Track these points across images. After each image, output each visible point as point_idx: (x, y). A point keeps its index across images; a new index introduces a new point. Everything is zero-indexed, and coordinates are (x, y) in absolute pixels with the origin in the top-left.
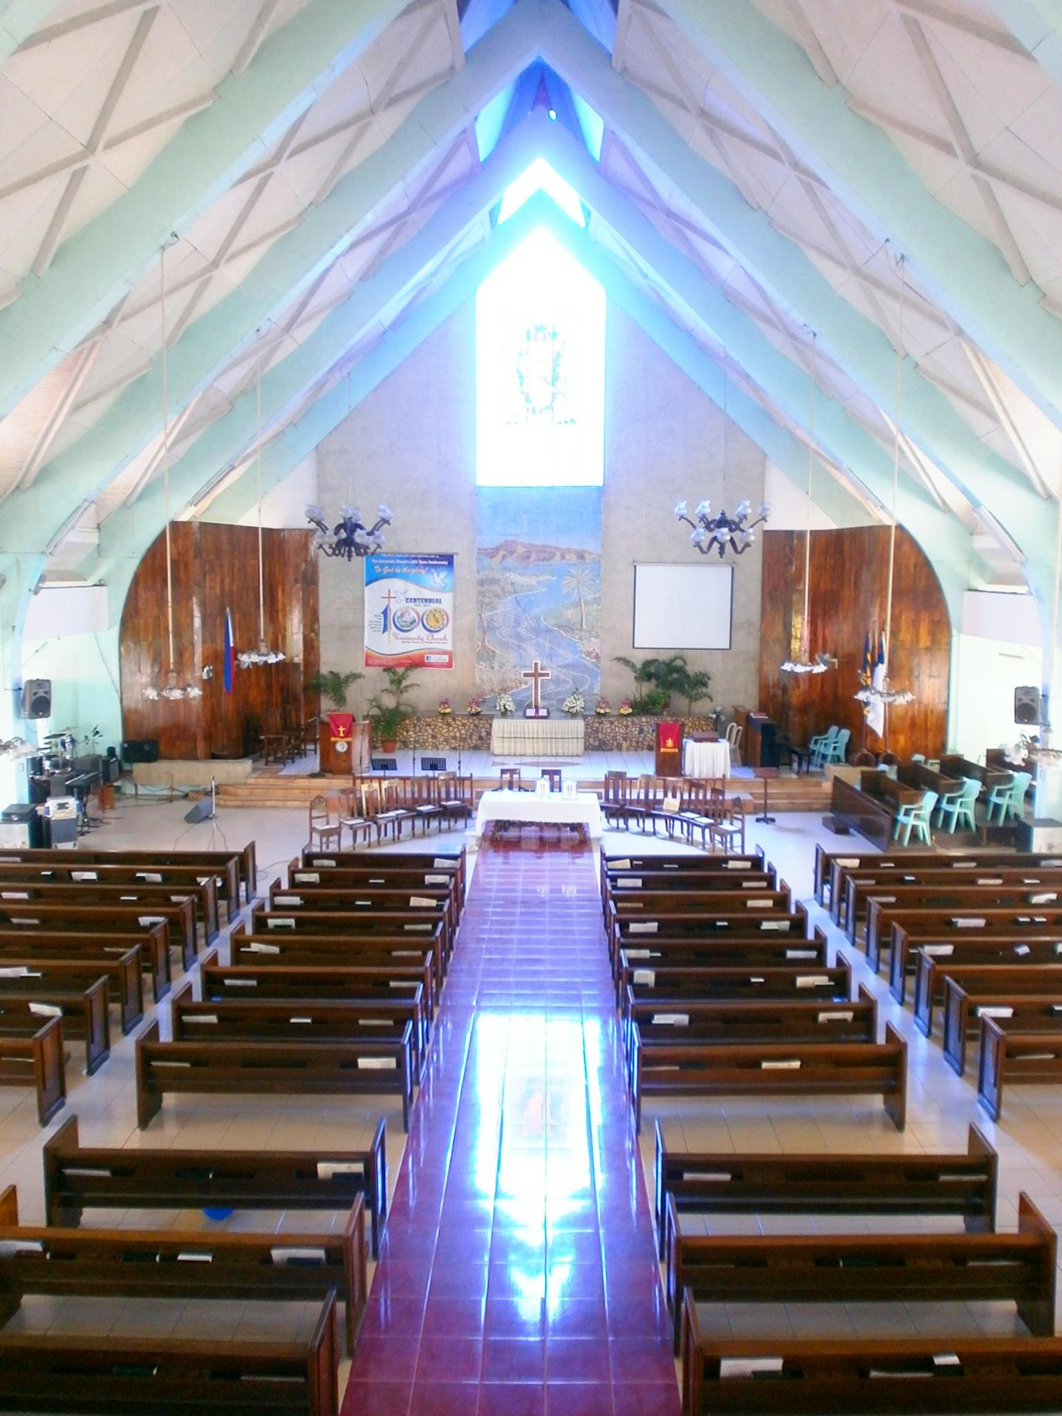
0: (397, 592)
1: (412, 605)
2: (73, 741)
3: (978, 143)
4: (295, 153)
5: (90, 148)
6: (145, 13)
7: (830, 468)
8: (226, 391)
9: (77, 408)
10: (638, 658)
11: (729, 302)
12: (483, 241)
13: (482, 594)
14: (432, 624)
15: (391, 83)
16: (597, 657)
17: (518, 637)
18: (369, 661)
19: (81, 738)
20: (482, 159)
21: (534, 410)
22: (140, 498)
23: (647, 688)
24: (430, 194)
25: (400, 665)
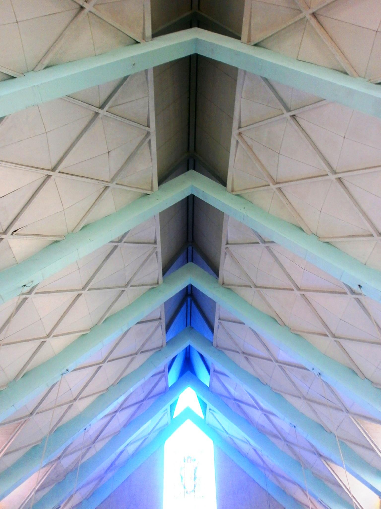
3: (333, 330)
4: (108, 362)
5: (48, 336)
6: (79, 294)
8: (65, 467)
11: (260, 432)
12: (167, 424)
15: (143, 345)
21: (187, 492)
24: (150, 396)
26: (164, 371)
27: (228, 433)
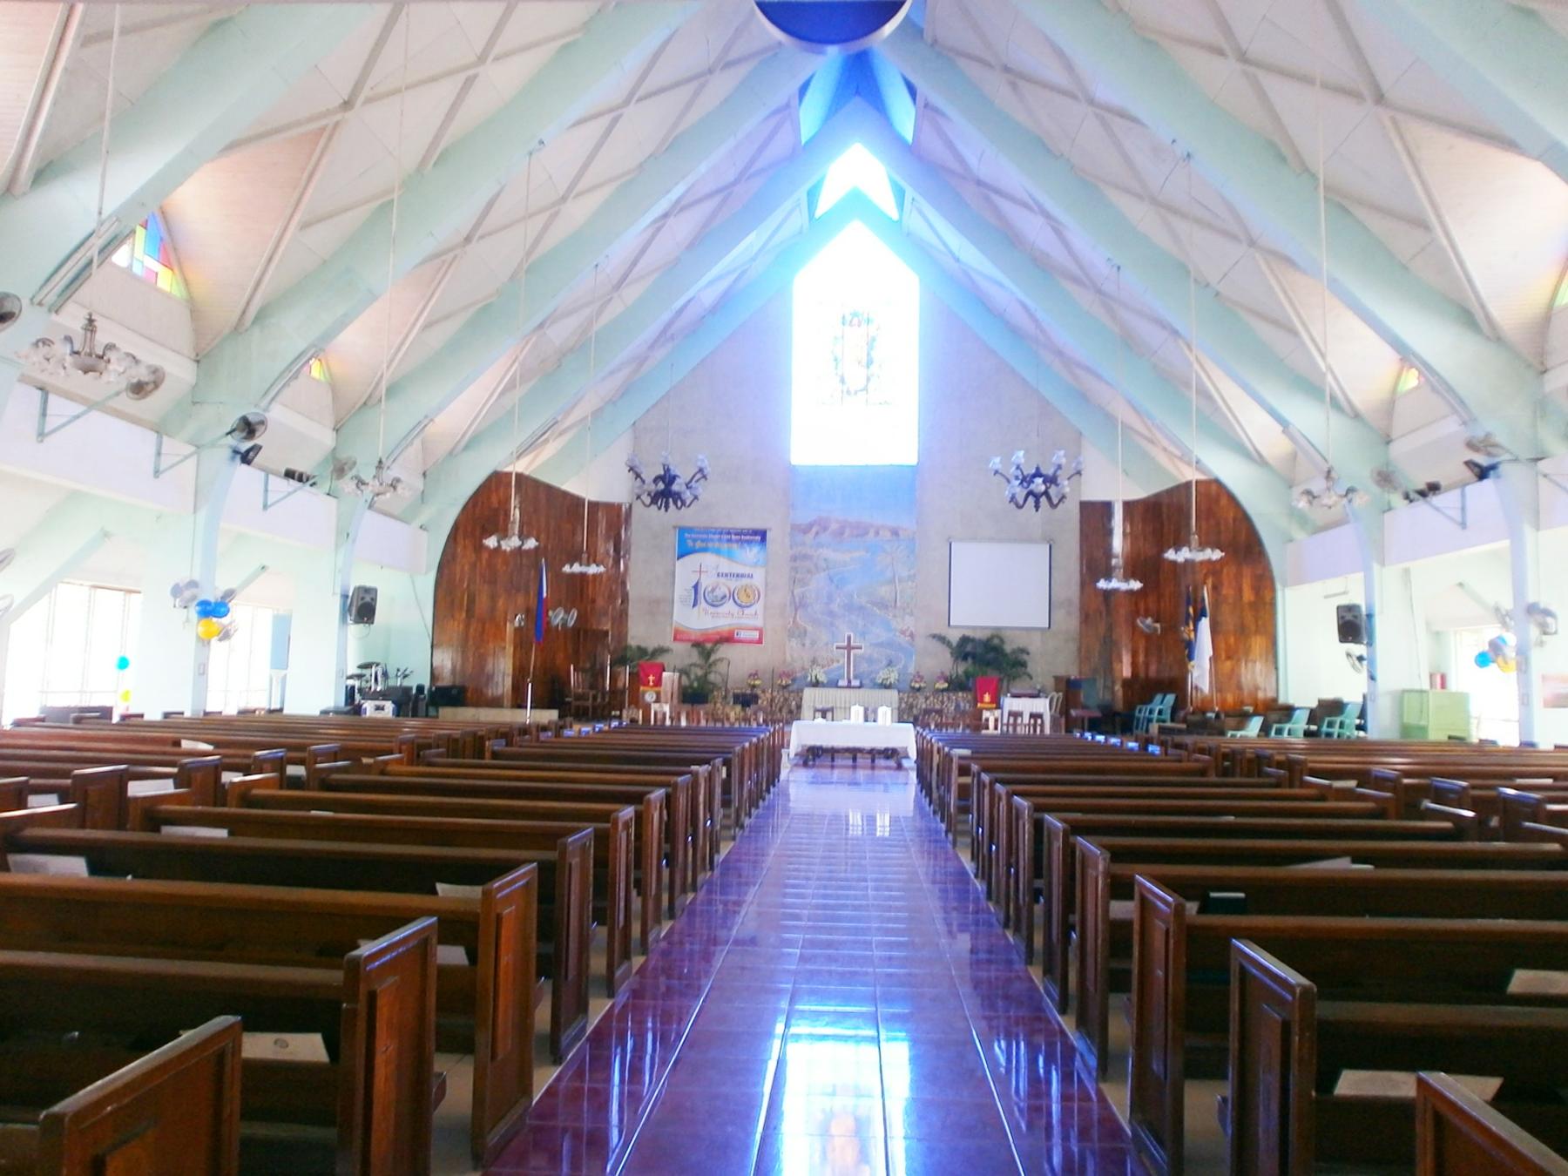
0: (708, 566)
1: (722, 580)
2: (385, 674)
4: (640, 100)
5: (482, 59)
7: (1144, 443)
9: (428, 326)
10: (954, 637)
11: (1039, 265)
13: (795, 570)
14: (743, 599)
15: (727, 48)
16: (912, 635)
17: (831, 614)
18: (678, 636)
19: (392, 673)
20: (804, 141)
22: (466, 448)
23: (962, 668)
24: (752, 170)
25: (708, 640)
26: (788, 106)
27: (957, 260)
